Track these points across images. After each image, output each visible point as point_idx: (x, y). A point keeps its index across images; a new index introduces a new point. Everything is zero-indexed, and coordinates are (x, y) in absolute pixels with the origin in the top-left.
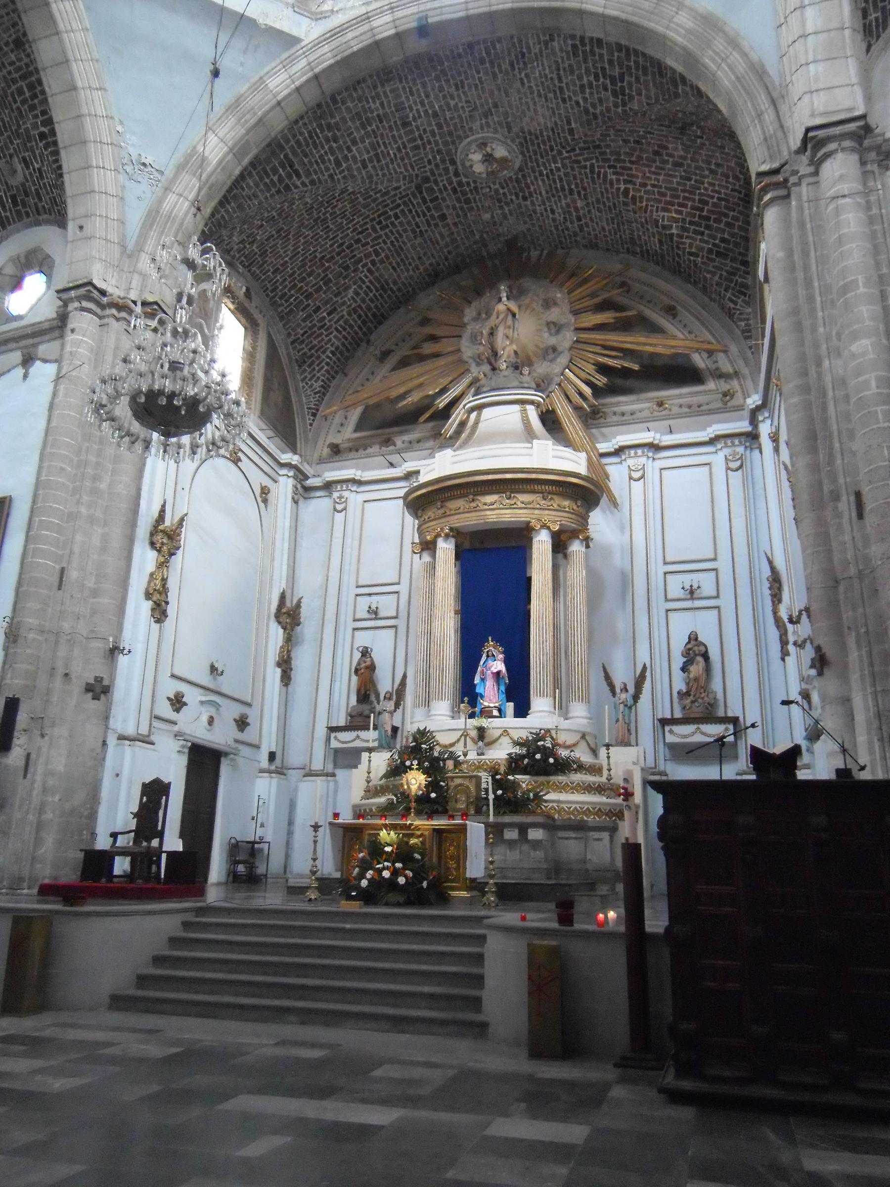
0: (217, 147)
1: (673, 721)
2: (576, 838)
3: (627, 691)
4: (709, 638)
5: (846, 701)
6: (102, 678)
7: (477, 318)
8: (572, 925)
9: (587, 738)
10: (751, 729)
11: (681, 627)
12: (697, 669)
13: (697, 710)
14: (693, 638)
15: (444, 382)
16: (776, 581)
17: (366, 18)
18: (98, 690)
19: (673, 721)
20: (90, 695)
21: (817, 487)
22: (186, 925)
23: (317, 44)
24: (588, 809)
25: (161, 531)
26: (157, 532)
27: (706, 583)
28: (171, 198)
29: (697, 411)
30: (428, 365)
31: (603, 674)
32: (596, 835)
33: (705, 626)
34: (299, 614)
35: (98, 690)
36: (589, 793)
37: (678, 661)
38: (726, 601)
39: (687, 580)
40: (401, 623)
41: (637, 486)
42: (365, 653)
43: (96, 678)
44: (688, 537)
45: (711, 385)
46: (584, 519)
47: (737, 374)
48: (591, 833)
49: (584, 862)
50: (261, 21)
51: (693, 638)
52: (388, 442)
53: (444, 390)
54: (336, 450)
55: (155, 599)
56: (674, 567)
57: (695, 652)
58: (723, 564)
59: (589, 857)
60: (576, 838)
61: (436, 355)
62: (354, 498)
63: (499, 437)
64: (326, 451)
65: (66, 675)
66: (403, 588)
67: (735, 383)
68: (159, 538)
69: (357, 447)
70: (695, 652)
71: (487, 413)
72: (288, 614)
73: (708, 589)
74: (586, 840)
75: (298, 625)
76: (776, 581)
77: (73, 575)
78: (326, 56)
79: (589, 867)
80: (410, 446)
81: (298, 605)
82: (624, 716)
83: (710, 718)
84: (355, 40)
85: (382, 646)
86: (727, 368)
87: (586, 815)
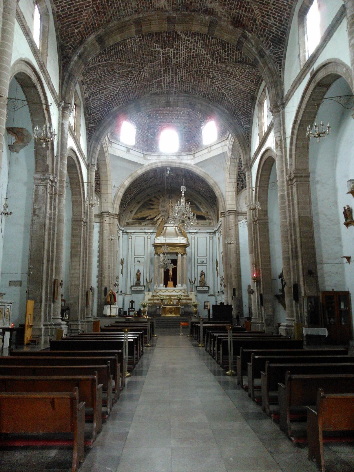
0: (127, 183)
1: (198, 286)
4: (205, 271)
5: (227, 291)
7: (162, 202)
8: (231, 306)
11: (200, 269)
12: (203, 277)
13: (203, 285)
14: (202, 271)
15: (155, 215)
16: (217, 263)
17: (157, 163)
19: (198, 286)
21: (226, 262)
23: (147, 166)
27: (205, 260)
28: (119, 193)
29: (204, 226)
30: (152, 211)
33: (204, 268)
37: (199, 275)
38: (208, 264)
39: (202, 260)
40: (145, 264)
41: (193, 240)
44: (202, 252)
45: (207, 221)
46: (186, 250)
47: (212, 219)
50: (139, 162)
51: (202, 271)
52: (140, 223)
53: (155, 217)
54: (128, 224)
56: (199, 257)
57: (202, 274)
58: (208, 257)
61: (153, 209)
62: (133, 236)
63: (171, 234)
64: (126, 224)
66: (145, 257)
67: (212, 221)
69: (133, 224)
70: (202, 274)
71: (168, 228)
73: (205, 262)
76: (217, 263)
78: (149, 168)
80: (146, 225)
83: (204, 286)
84: (154, 166)
85: (141, 268)
86: (210, 218)
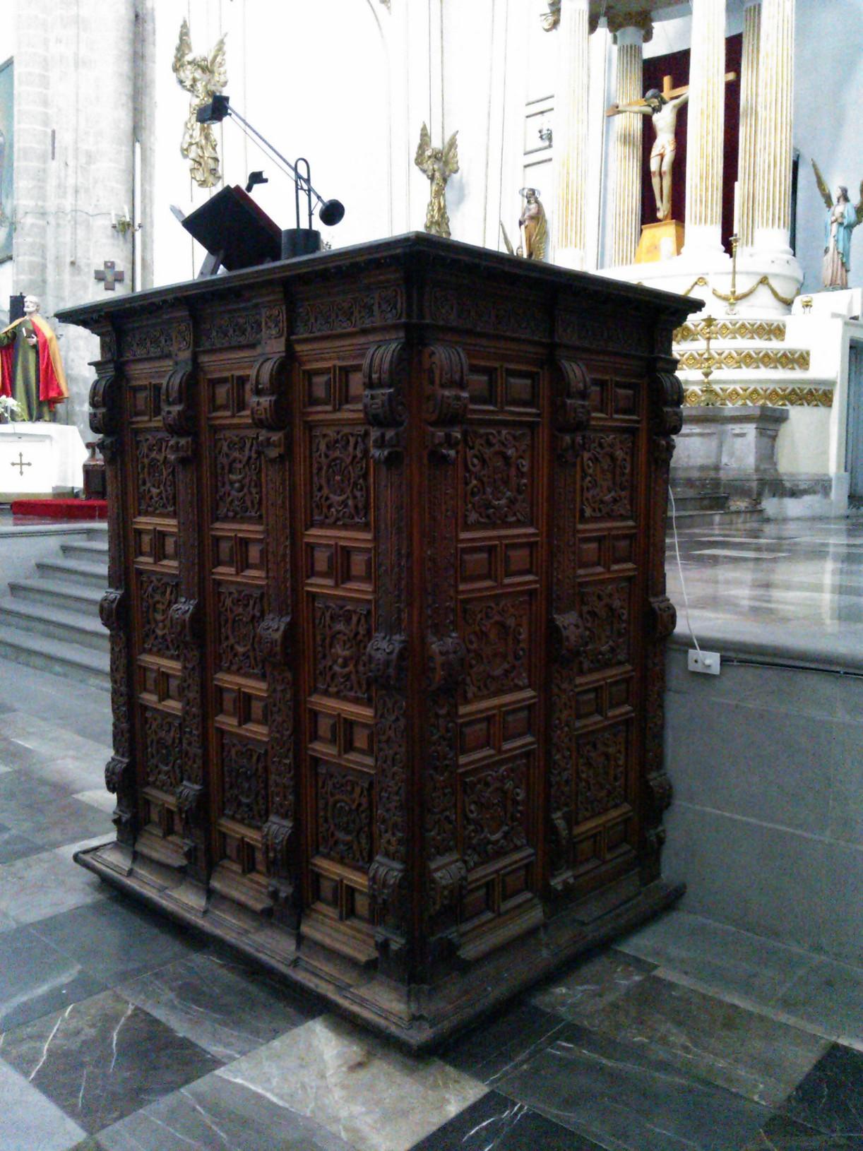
2: (701, 435)
3: (846, 199)
6: (113, 263)
9: (772, 281)
10: (256, 187)
18: (110, 277)
20: (102, 285)
22: (66, 550)
24: (774, 391)
25: (189, 63)
26: (182, 66)
31: (814, 179)
32: (737, 428)
34: (455, 156)
35: (110, 277)
36: (766, 366)
42: (531, 196)
43: (106, 263)
48: (730, 426)
49: (717, 468)
55: (192, 155)
59: (725, 460)
60: (701, 435)
65: (73, 263)
68: (188, 74)
72: (437, 157)
74: (722, 434)
75: (456, 171)
77: (65, 138)
79: (722, 475)
81: (452, 144)
82: (837, 241)
87: (771, 400)
